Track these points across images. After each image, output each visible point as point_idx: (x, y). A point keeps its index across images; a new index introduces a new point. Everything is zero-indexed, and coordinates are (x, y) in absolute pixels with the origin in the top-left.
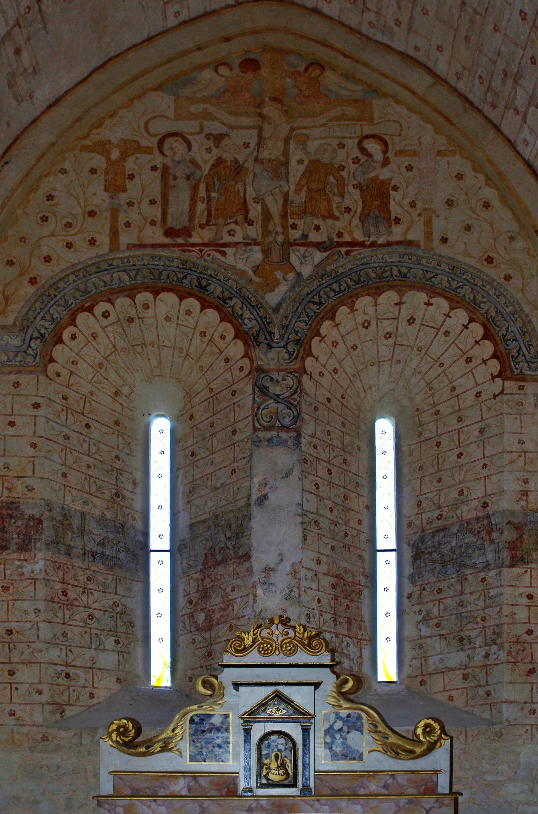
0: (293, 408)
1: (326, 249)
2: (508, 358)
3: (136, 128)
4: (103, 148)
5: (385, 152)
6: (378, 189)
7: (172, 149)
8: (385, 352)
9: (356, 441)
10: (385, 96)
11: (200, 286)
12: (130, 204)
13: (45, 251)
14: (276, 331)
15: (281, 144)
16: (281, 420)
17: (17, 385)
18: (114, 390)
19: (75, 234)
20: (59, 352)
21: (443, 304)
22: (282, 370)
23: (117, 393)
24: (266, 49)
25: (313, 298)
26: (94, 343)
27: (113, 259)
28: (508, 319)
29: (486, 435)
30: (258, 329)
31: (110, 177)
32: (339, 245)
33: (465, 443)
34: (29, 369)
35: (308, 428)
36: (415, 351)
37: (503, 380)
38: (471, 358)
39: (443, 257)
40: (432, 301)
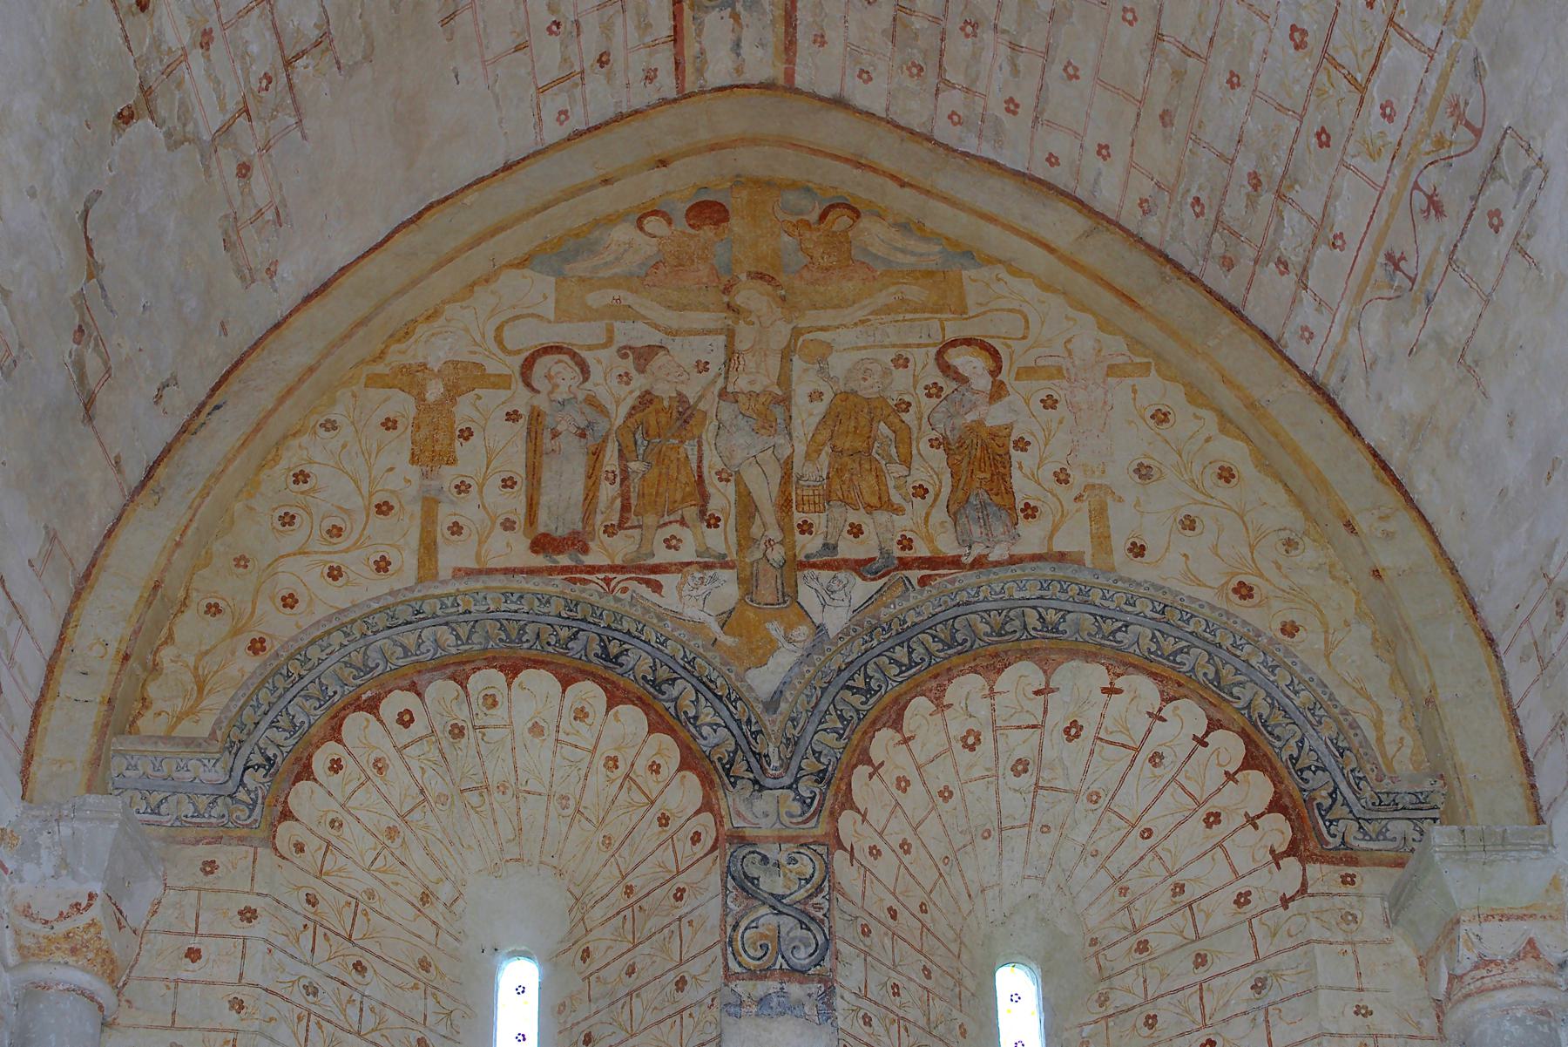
0: (813, 926)
1: (877, 575)
2: (1310, 811)
3: (478, 338)
4: (411, 378)
5: (995, 372)
6: (985, 448)
7: (548, 377)
8: (1016, 807)
9: (955, 1013)
10: (991, 261)
11: (606, 656)
12: (462, 488)
13: (285, 584)
14: (772, 750)
15: (774, 363)
16: (788, 954)
17: (209, 867)
18: (419, 891)
19: (347, 550)
20: (303, 798)
21: (1144, 689)
22: (789, 840)
23: (425, 898)
24: (739, 181)
25: (852, 678)
26: (378, 781)
27: (423, 599)
28: (1301, 720)
29: (1272, 995)
30: (732, 748)
31: (424, 432)
32: (905, 564)
33: (1218, 1017)
34: (238, 833)
35: (850, 976)
36: (1083, 803)
37: (1303, 861)
38: (1218, 815)
39: (1139, 584)
40: (1119, 683)
